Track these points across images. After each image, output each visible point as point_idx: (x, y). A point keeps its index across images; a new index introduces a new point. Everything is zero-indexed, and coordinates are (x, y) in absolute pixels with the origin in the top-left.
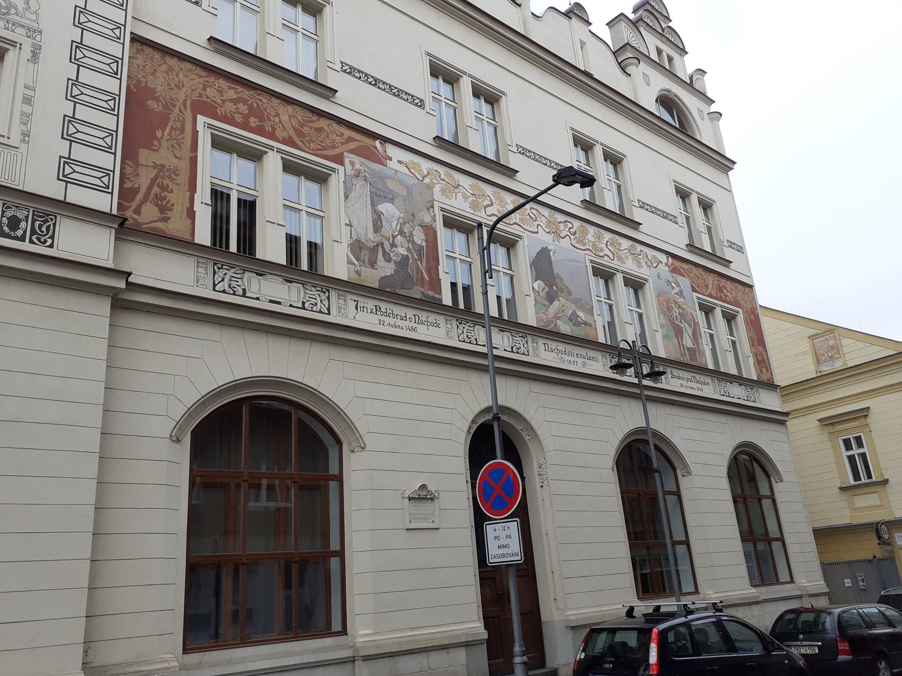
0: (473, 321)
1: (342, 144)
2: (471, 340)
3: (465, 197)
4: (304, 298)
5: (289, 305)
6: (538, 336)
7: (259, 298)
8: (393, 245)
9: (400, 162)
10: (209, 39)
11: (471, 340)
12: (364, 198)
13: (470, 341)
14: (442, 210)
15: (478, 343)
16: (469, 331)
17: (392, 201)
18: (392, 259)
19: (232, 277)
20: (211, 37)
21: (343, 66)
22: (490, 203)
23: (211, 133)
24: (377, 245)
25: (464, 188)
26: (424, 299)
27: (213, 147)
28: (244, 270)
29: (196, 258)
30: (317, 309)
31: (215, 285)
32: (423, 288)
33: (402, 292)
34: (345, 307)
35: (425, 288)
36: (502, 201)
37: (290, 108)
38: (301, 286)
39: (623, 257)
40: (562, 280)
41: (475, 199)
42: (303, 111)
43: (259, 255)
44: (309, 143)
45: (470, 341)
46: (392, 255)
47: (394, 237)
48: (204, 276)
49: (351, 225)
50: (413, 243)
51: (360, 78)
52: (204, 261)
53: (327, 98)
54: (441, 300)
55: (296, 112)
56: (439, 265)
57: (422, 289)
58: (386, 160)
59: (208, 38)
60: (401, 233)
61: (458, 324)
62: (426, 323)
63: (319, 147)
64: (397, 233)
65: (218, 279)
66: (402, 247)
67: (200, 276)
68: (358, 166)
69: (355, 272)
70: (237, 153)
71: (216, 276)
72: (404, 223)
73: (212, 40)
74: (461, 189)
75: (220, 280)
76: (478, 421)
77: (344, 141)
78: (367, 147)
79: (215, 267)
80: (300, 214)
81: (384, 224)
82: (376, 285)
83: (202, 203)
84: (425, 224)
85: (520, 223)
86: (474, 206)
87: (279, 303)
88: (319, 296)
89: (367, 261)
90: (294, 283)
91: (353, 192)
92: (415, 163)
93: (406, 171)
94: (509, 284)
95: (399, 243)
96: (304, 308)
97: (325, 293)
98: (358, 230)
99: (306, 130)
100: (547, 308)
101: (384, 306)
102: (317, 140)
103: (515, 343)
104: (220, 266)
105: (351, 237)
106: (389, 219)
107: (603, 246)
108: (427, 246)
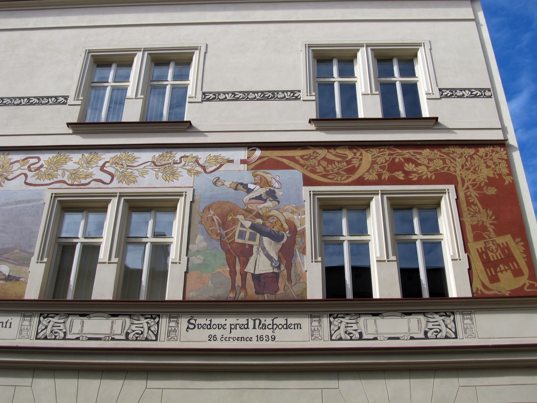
2: (351, 335)
4: (128, 329)
5: (409, 338)
7: (377, 337)
11: (351, 335)
13: (351, 337)
16: (349, 325)
19: (55, 323)
52: (318, 315)
65: (41, 327)
83: (180, 263)
87: (398, 338)
96: (426, 337)
97: (154, 319)
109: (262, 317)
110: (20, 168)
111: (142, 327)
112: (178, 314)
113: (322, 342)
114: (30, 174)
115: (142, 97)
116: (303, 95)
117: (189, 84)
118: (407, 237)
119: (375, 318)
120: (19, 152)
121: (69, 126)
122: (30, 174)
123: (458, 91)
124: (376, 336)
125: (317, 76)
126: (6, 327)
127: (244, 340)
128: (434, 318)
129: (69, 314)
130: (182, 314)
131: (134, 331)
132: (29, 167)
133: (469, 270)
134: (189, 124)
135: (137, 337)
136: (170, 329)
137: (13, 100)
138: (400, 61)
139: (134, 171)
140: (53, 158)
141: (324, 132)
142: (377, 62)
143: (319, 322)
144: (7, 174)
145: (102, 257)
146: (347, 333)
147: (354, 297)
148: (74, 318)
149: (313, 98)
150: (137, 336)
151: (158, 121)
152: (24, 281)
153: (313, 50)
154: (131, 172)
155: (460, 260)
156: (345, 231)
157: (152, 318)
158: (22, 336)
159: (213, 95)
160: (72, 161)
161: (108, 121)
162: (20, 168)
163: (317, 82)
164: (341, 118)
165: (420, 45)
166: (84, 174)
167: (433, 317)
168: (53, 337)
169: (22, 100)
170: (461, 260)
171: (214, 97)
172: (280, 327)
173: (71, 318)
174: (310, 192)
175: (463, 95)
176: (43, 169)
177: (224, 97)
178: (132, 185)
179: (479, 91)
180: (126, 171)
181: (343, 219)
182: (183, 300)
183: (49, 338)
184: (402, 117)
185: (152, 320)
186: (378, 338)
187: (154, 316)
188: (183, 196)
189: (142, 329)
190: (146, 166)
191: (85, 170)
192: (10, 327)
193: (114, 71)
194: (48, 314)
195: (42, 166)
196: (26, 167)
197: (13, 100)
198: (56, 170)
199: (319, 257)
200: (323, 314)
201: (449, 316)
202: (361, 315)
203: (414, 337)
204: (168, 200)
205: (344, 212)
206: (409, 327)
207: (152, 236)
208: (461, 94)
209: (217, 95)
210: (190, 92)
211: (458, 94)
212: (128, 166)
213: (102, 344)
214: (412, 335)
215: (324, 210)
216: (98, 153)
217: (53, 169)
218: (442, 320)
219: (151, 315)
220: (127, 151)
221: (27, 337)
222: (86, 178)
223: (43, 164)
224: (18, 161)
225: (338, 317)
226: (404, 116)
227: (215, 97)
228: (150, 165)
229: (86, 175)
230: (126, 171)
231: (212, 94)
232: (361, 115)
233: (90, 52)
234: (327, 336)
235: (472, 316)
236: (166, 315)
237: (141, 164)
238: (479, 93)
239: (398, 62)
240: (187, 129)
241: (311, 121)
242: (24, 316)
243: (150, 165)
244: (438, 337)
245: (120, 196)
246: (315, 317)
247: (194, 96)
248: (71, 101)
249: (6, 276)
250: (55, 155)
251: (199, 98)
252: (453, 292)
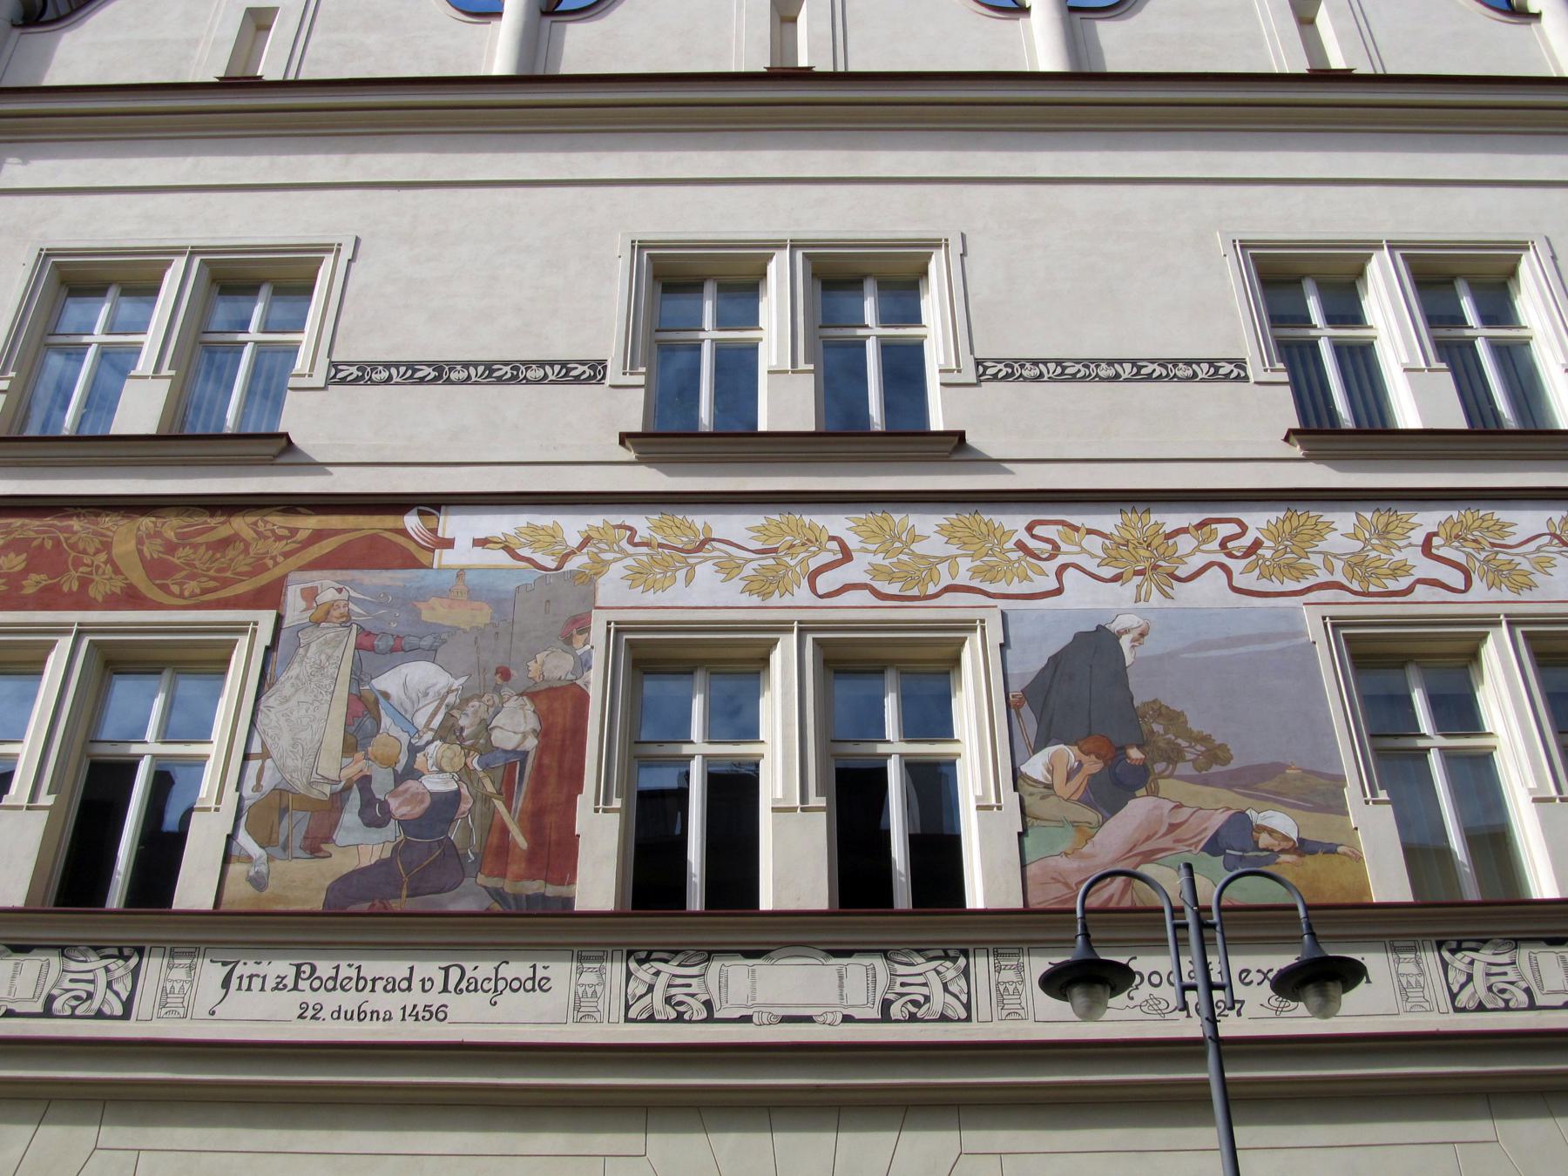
2: (1506, 996)
3: (728, 568)
11: (1506, 996)
12: (331, 670)
13: (1507, 1001)
19: (674, 976)
24: (347, 789)
26: (497, 908)
29: (1387, 940)
31: (1453, 996)
39: (1525, 565)
40: (1173, 718)
41: (771, 562)
45: (1507, 1001)
56: (580, 791)
60: (449, 731)
63: (212, 584)
65: (637, 988)
66: (441, 771)
67: (585, 992)
68: (328, 596)
71: (1451, 974)
74: (714, 549)
75: (1463, 979)
83: (217, 810)
85: (975, 583)
87: (809, 1019)
88: (938, 973)
93: (502, 558)
96: (886, 1017)
100: (1085, 833)
103: (903, 985)
104: (1454, 945)
107: (1414, 557)
108: (542, 750)
109: (468, 959)
110: (1197, 549)
111: (925, 985)
112: (1019, 946)
113: (605, 1027)
114: (1236, 566)
115: (173, 373)
116: (1254, 371)
117: (761, 339)
118: (864, 748)
119: (751, 962)
120: (1174, 505)
121: (627, 443)
122: (1236, 566)
123: (1181, 365)
125: (821, 323)
126: (374, 991)
129: (710, 953)
132: (1223, 545)
133: (229, 837)
134: (284, 442)
136: (580, 990)
137: (1092, 366)
138: (1324, 290)
139: (1517, 559)
140: (1280, 523)
141: (1325, 464)
142: (822, 289)
144: (1167, 564)
145: (204, 796)
146: (670, 1005)
147: (914, 905)
148: (727, 963)
149: (641, 380)
150: (74, 1003)
151: (263, 431)
152: (1350, 853)
153: (1254, 257)
154: (1510, 562)
155: (999, 808)
156: (1425, 723)
157: (946, 957)
158: (1009, 1011)
159: (433, 370)
160: (1336, 530)
161: (80, 434)
162: (1197, 549)
163: (820, 337)
164: (712, 430)
165: (935, 244)
166: (1387, 566)
168: (673, 1015)
169: (472, 370)
170: (1001, 809)
171: (360, 374)
172: (516, 985)
173: (720, 963)
174: (609, 623)
175: (1195, 375)
176: (1266, 553)
178: (1526, 595)
179: (1159, 365)
180: (1494, 559)
181: (695, 697)
182: (215, 911)
183: (657, 1017)
184: (1510, 428)
188: (248, 631)
190: (1541, 546)
191: (1383, 556)
192: (238, 990)
193: (264, 306)
194: (650, 953)
195: (1257, 544)
196: (1215, 545)
197: (523, 368)
198: (1303, 554)
199: (616, 797)
201: (954, 960)
204: (1444, 636)
205: (700, 678)
206: (841, 986)
207: (157, 738)
208: (1111, 372)
209: (369, 369)
210: (301, 363)
211: (1179, 374)
212: (1493, 545)
213: (701, 1032)
215: (837, 672)
216: (1396, 511)
217: (1292, 552)
218: (935, 970)
220: (1474, 505)
221: (181, 1011)
222: (1395, 573)
223: (1257, 537)
224: (1184, 531)
225: (652, 957)
226: (1513, 425)
227: (363, 375)
228: (1550, 544)
229: (1392, 567)
230: (1494, 559)
232: (762, 427)
233: (50, 253)
235: (1021, 960)
236: (986, 951)
237: (1524, 539)
238: (1159, 370)
239: (1319, 289)
240: (275, 457)
241: (624, 438)
242: (173, 955)
243: (1550, 544)
244: (78, 1012)
245: (80, 633)
246: (588, 959)
247: (307, 372)
248: (614, 374)
249: (1294, 841)
250: (1281, 515)
251: (319, 379)
252: (976, 896)
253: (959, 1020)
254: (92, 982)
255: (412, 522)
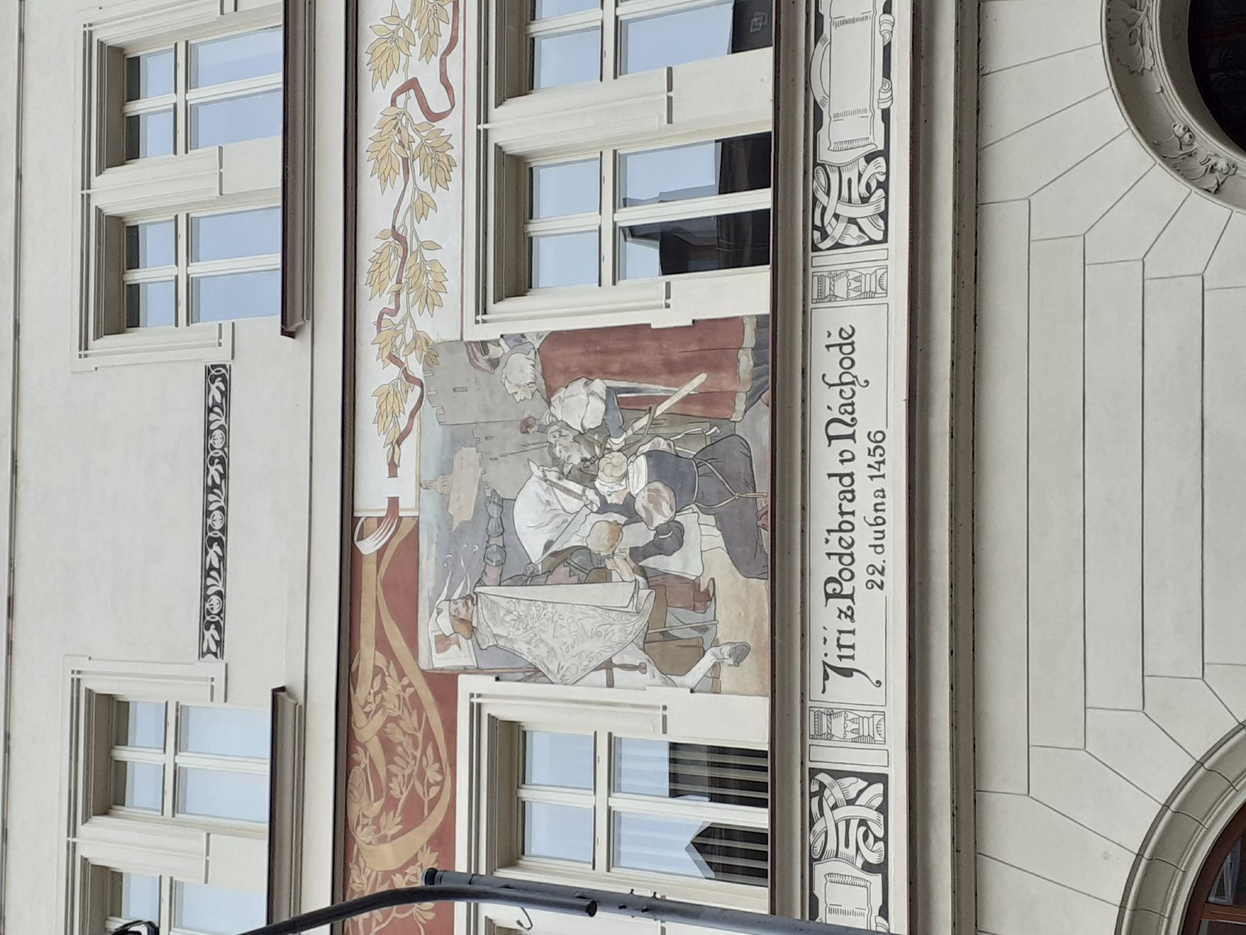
0: (806, 172)
1: (401, 675)
2: (874, 185)
3: (423, 207)
4: (853, 864)
6: (805, 270)
7: (883, 111)
8: (628, 509)
9: (393, 468)
10: (292, 335)
11: (874, 185)
12: (521, 608)
14: (481, 308)
15: (881, 147)
16: (845, 193)
17: (505, 505)
18: (672, 520)
20: (284, 333)
21: (209, 651)
22: (412, 92)
23: (495, 303)
24: (643, 571)
25: (397, 211)
26: (767, 395)
27: (532, 88)
28: (815, 164)
30: (877, 823)
31: (872, 242)
32: (734, 394)
33: (764, 486)
34: (851, 716)
35: (732, 388)
36: (393, 38)
37: (362, 836)
38: (820, 869)
41: (417, 162)
42: (356, 793)
43: (769, 128)
44: (430, 785)
46: (659, 520)
47: (605, 507)
48: (852, 721)
49: (608, 665)
50: (604, 430)
51: (220, 594)
52: (812, 717)
53: (301, 713)
54: (760, 320)
55: (365, 816)
56: (649, 325)
57: (740, 405)
58: (401, 518)
59: (291, 339)
60: (586, 476)
61: (828, 243)
62: (848, 394)
63: (430, 751)
64: (590, 494)
66: (626, 475)
69: (737, 663)
70: (528, 24)
72: (556, 461)
73: (291, 329)
74: (404, 225)
75: (855, 228)
76: (1179, 131)
77: (392, 664)
78: (388, 585)
79: (823, 246)
80: (628, 21)
81: (575, 541)
82: (763, 587)
84: (541, 380)
86: (439, 168)
87: (887, 49)
89: (697, 618)
90: (821, 11)
91: (516, 647)
92: (380, 414)
93: (409, 444)
94: (640, 243)
95: (617, 488)
96: (881, 868)
97: (823, 786)
98: (616, 639)
99: (399, 790)
101: (823, 567)
102: (415, 758)
105: (641, 668)
106: (559, 520)
108: (606, 374)
124: (879, 114)
127: (883, 504)
128: (826, 833)
130: (810, 266)
131: (858, 849)
135: (876, 839)
136: (853, 294)
143: (834, 276)
146: (869, 198)
150: (871, 839)
167: (823, 836)
172: (847, 363)
177: (218, 514)
185: (827, 793)
186: (885, 106)
187: (815, 788)
189: (854, 824)
200: (812, 267)
202: (818, 161)
203: (881, 907)
208: (218, 434)
214: (876, 912)
219: (812, 795)
231: (205, 632)
234: (876, 252)
244: (880, 834)
253: (885, 794)
254: (848, 822)
255: (368, 547)
